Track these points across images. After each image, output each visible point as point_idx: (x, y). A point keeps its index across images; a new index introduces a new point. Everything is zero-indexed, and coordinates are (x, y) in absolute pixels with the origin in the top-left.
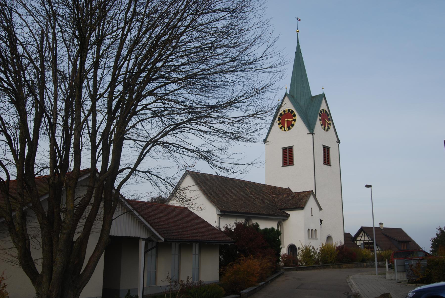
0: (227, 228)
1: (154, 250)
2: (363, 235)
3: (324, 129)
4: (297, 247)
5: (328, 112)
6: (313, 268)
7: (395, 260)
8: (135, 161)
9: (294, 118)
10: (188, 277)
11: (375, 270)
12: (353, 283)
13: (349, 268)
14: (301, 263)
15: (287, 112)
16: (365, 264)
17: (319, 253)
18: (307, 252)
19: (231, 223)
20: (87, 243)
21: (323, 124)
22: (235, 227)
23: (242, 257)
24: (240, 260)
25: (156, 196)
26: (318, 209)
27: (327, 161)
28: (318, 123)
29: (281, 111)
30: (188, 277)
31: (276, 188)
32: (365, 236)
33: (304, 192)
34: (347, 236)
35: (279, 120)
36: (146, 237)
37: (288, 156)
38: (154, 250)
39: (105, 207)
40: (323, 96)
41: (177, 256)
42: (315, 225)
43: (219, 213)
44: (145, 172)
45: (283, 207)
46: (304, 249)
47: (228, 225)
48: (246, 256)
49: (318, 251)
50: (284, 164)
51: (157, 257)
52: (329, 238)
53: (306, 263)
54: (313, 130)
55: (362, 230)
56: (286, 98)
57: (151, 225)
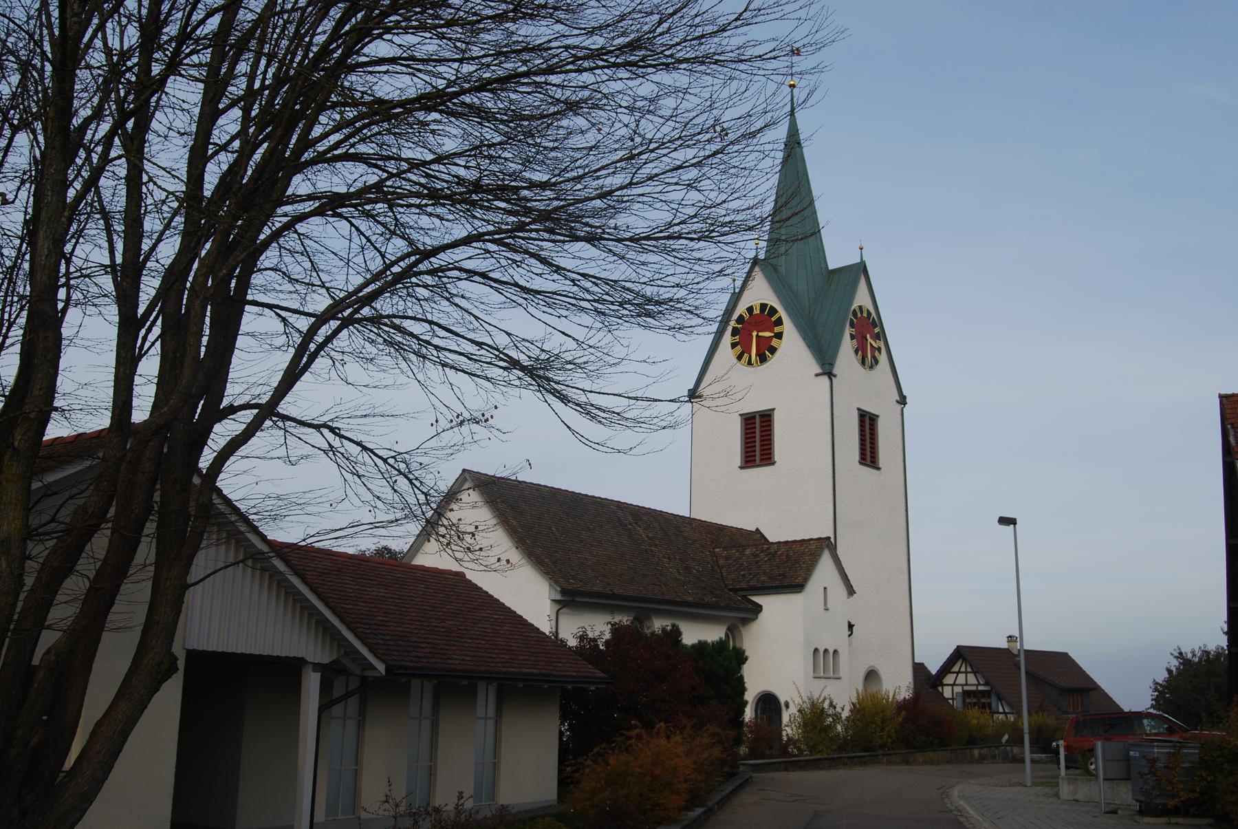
0: (582, 638)
1: (353, 702)
2: (963, 669)
3: (863, 363)
4: (782, 702)
5: (874, 314)
6: (834, 763)
7: (1099, 744)
8: (275, 381)
9: (777, 329)
10: (461, 793)
11: (1024, 770)
12: (971, 811)
13: (932, 763)
14: (799, 749)
15: (757, 311)
16: (976, 752)
17: (848, 719)
18: (815, 717)
19: (599, 626)
20: (90, 671)
21: (861, 350)
22: (608, 636)
23: (636, 727)
24: (630, 738)
25: (374, 547)
26: (844, 592)
27: (869, 455)
28: (847, 346)
29: (741, 309)
30: (461, 793)
31: (721, 529)
32: (966, 672)
33: (803, 540)
34: (919, 669)
35: (733, 334)
36: (326, 660)
37: (758, 438)
38: (353, 702)
39: (160, 538)
40: (861, 269)
41: (426, 724)
42: (833, 638)
43: (559, 597)
44: (318, 427)
45: (743, 585)
46: (806, 706)
47: (589, 629)
48: (648, 726)
49: (845, 714)
50: (747, 462)
51: (361, 725)
52: (871, 675)
53: (812, 749)
54: (832, 365)
55: (961, 655)
56: (757, 269)
57: (342, 621)
